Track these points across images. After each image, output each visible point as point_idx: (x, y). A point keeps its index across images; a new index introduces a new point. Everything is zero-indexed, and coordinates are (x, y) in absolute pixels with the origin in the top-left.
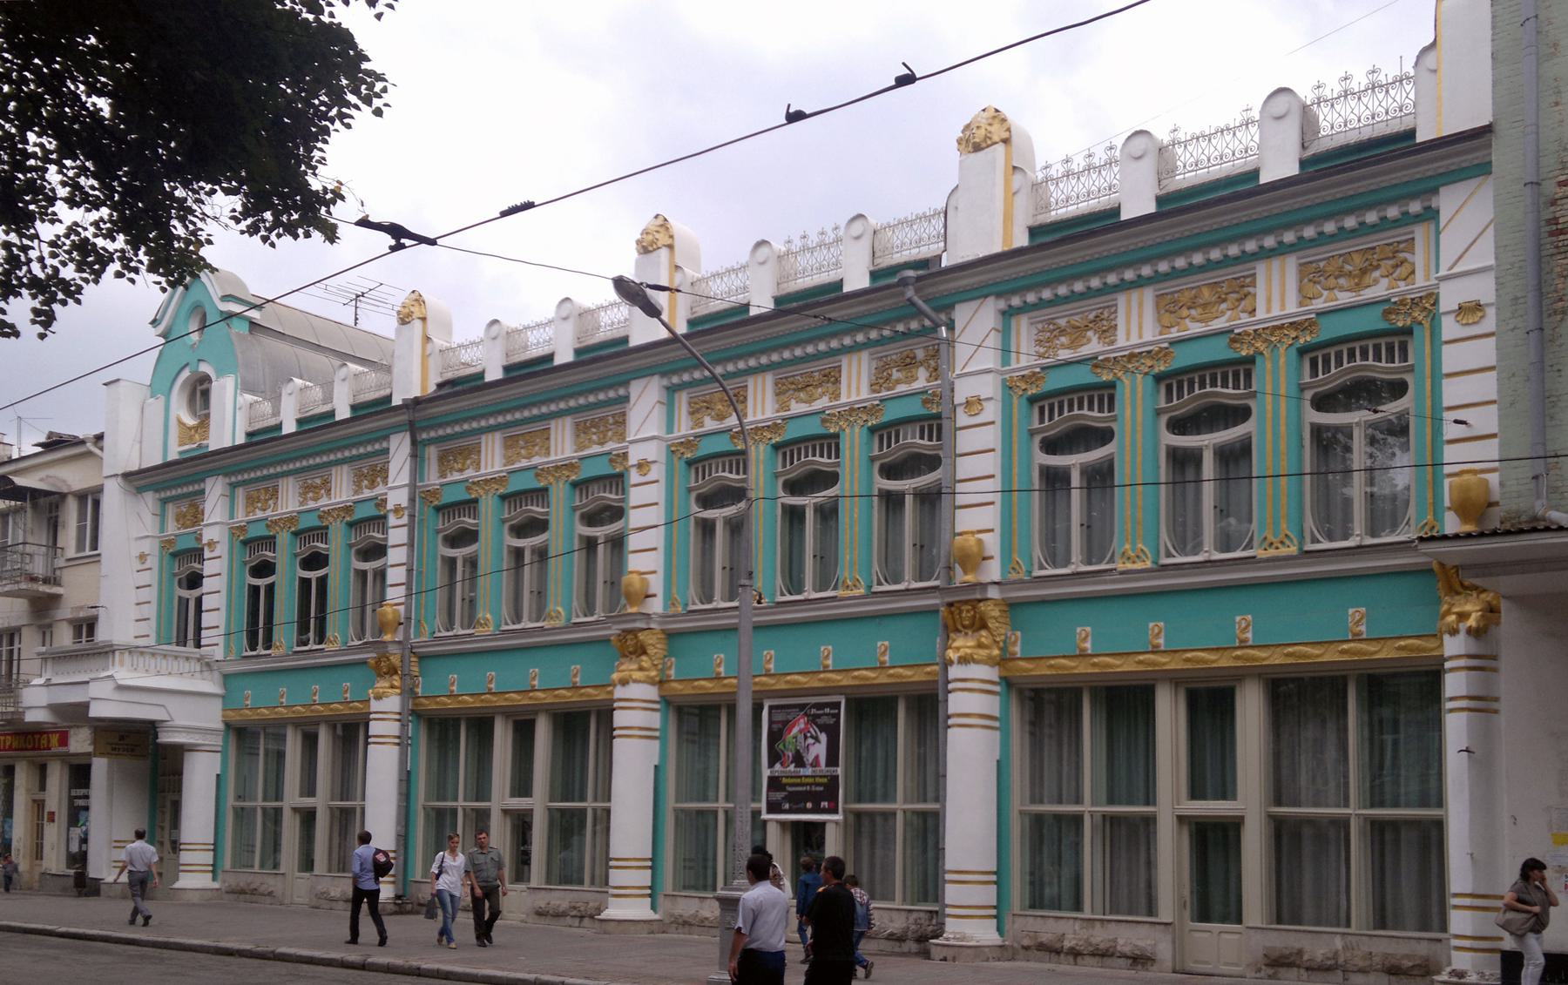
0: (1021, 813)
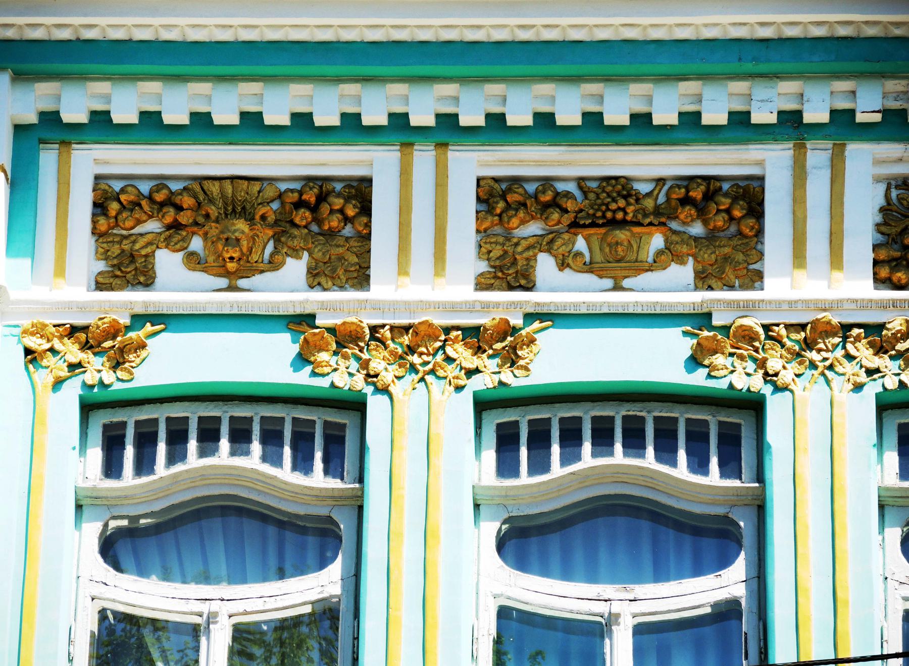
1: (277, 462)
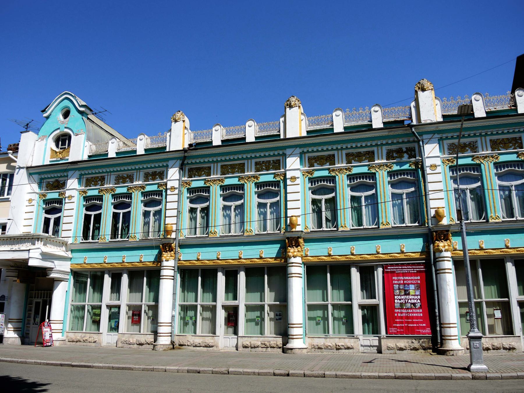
0: (180, 305)
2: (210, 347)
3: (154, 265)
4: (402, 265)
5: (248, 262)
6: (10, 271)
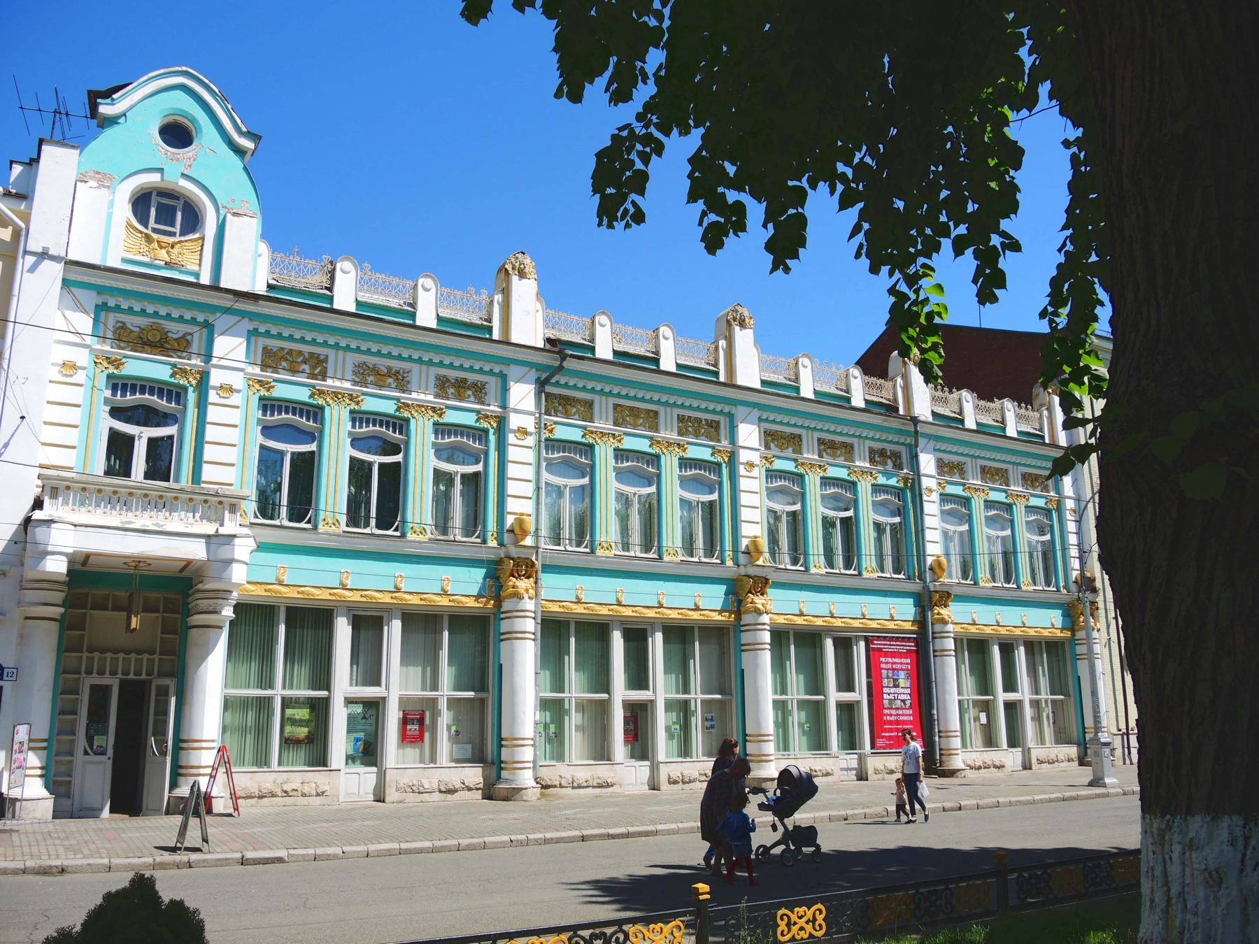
1: (382, 427)
2: (609, 785)
3: (478, 605)
4: (892, 639)
5: (414, 600)
6: (211, 595)
